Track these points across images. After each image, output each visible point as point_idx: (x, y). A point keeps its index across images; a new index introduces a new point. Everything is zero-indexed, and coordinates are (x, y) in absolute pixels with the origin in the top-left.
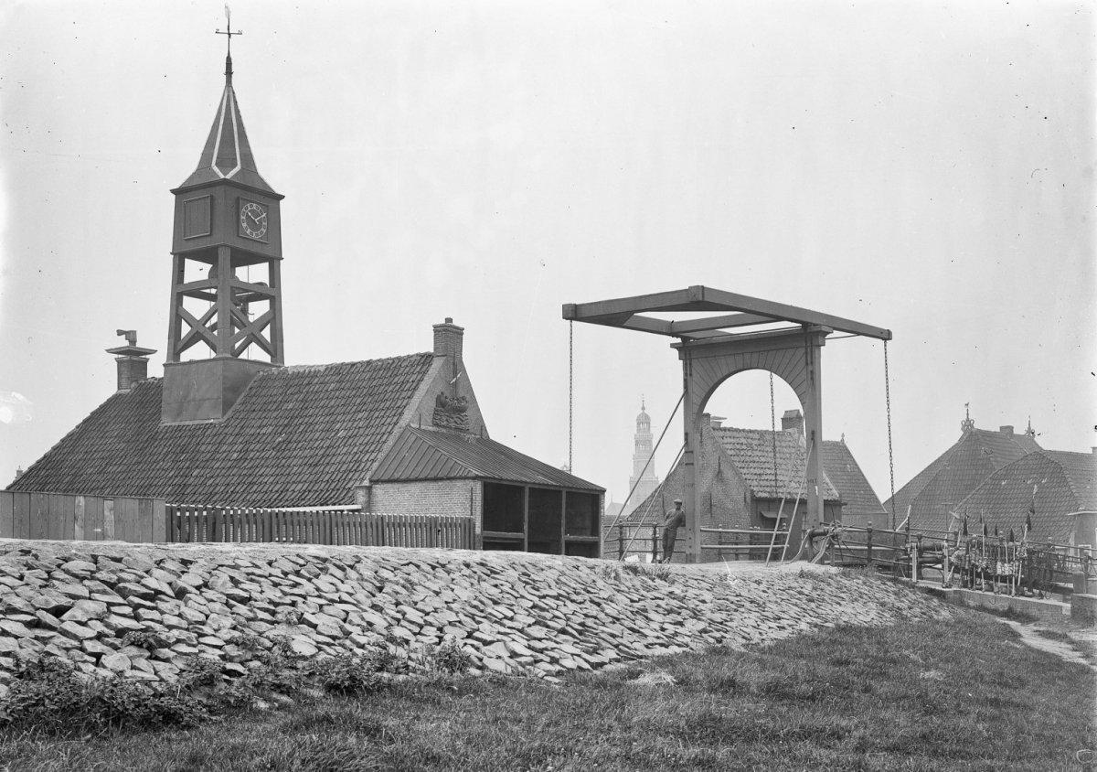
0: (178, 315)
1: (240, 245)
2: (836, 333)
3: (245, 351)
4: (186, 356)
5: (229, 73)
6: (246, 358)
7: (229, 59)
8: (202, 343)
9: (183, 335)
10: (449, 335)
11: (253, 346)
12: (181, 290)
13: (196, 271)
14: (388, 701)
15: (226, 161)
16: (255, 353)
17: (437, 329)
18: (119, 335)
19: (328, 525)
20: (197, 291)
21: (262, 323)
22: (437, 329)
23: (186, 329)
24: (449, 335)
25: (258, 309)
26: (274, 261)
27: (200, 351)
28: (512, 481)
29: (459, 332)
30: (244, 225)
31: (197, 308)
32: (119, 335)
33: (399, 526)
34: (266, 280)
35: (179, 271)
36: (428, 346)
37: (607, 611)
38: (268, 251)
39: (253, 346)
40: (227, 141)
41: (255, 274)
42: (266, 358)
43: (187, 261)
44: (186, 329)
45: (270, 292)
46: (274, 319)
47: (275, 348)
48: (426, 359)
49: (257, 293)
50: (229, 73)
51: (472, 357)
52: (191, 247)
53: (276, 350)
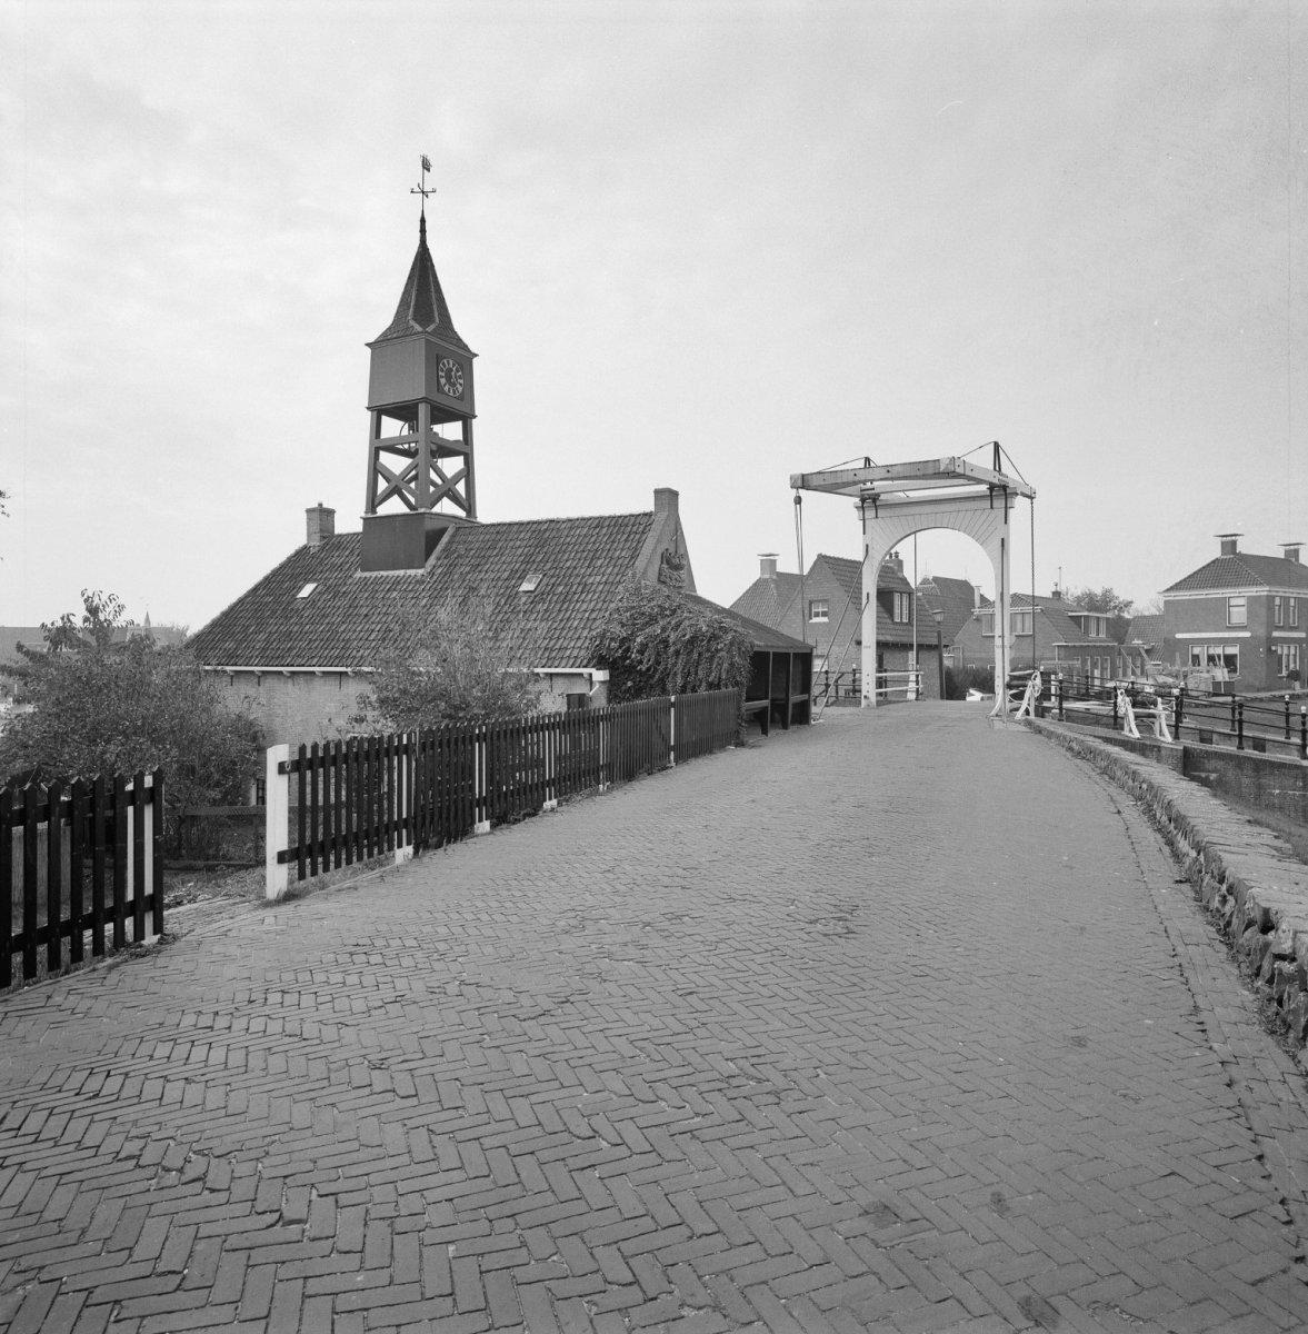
0: (376, 470)
1: (439, 399)
3: (439, 504)
4: (382, 510)
5: (423, 231)
6: (439, 511)
7: (423, 221)
9: (379, 492)
10: (667, 498)
12: (379, 446)
13: (392, 428)
14: (476, 692)
16: (446, 507)
17: (658, 492)
19: (119, 1065)
21: (456, 478)
22: (658, 492)
23: (382, 485)
24: (667, 498)
25: (451, 466)
26: (466, 418)
27: (394, 506)
28: (942, 688)
29: (675, 494)
30: (443, 381)
31: (396, 464)
33: (357, 760)
35: (377, 429)
37: (1123, 1060)
38: (466, 450)
41: (450, 431)
42: (462, 513)
43: (384, 418)
44: (382, 485)
45: (464, 448)
46: (468, 473)
47: (470, 506)
48: (647, 515)
49: (446, 450)
50: (423, 231)
52: (390, 398)
53: (470, 506)
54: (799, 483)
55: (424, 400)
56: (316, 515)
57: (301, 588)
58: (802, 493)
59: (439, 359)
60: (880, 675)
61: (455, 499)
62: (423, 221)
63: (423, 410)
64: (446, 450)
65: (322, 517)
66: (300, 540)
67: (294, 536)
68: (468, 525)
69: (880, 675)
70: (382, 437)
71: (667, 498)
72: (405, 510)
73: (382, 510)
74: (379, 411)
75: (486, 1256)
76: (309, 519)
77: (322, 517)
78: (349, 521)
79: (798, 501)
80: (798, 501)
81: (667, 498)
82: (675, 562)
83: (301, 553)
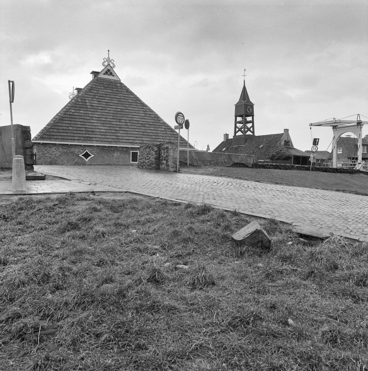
0: (236, 127)
1: (247, 114)
2: (365, 124)
4: (237, 134)
5: (244, 83)
7: (244, 81)
8: (240, 131)
11: (249, 131)
13: (239, 119)
15: (244, 99)
16: (249, 133)
17: (284, 130)
18: (27, 180)
20: (240, 123)
21: (251, 128)
22: (284, 130)
23: (237, 129)
25: (249, 125)
26: (253, 116)
27: (239, 133)
29: (288, 130)
30: (248, 110)
31: (239, 125)
32: (27, 180)
34: (251, 120)
36: (283, 132)
39: (249, 131)
40: (244, 90)
41: (249, 119)
42: (252, 134)
43: (237, 117)
44: (237, 129)
45: (252, 122)
46: (253, 126)
47: (253, 132)
48: (283, 134)
50: (244, 83)
51: (290, 133)
54: (311, 125)
55: (245, 114)
56: (226, 135)
57: (225, 150)
58: (311, 127)
59: (247, 107)
60: (301, 158)
61: (251, 131)
62: (244, 81)
63: (244, 116)
64: (249, 129)
65: (226, 135)
66: (223, 140)
67: (222, 140)
68: (253, 137)
69: (301, 158)
70: (237, 121)
71: (286, 131)
72: (242, 134)
73: (237, 134)
74: (236, 117)
75: (251, 161)
76: (224, 136)
77: (226, 135)
78: (231, 137)
79: (311, 128)
80: (311, 128)
81: (286, 131)
82: (288, 143)
83: (223, 142)
